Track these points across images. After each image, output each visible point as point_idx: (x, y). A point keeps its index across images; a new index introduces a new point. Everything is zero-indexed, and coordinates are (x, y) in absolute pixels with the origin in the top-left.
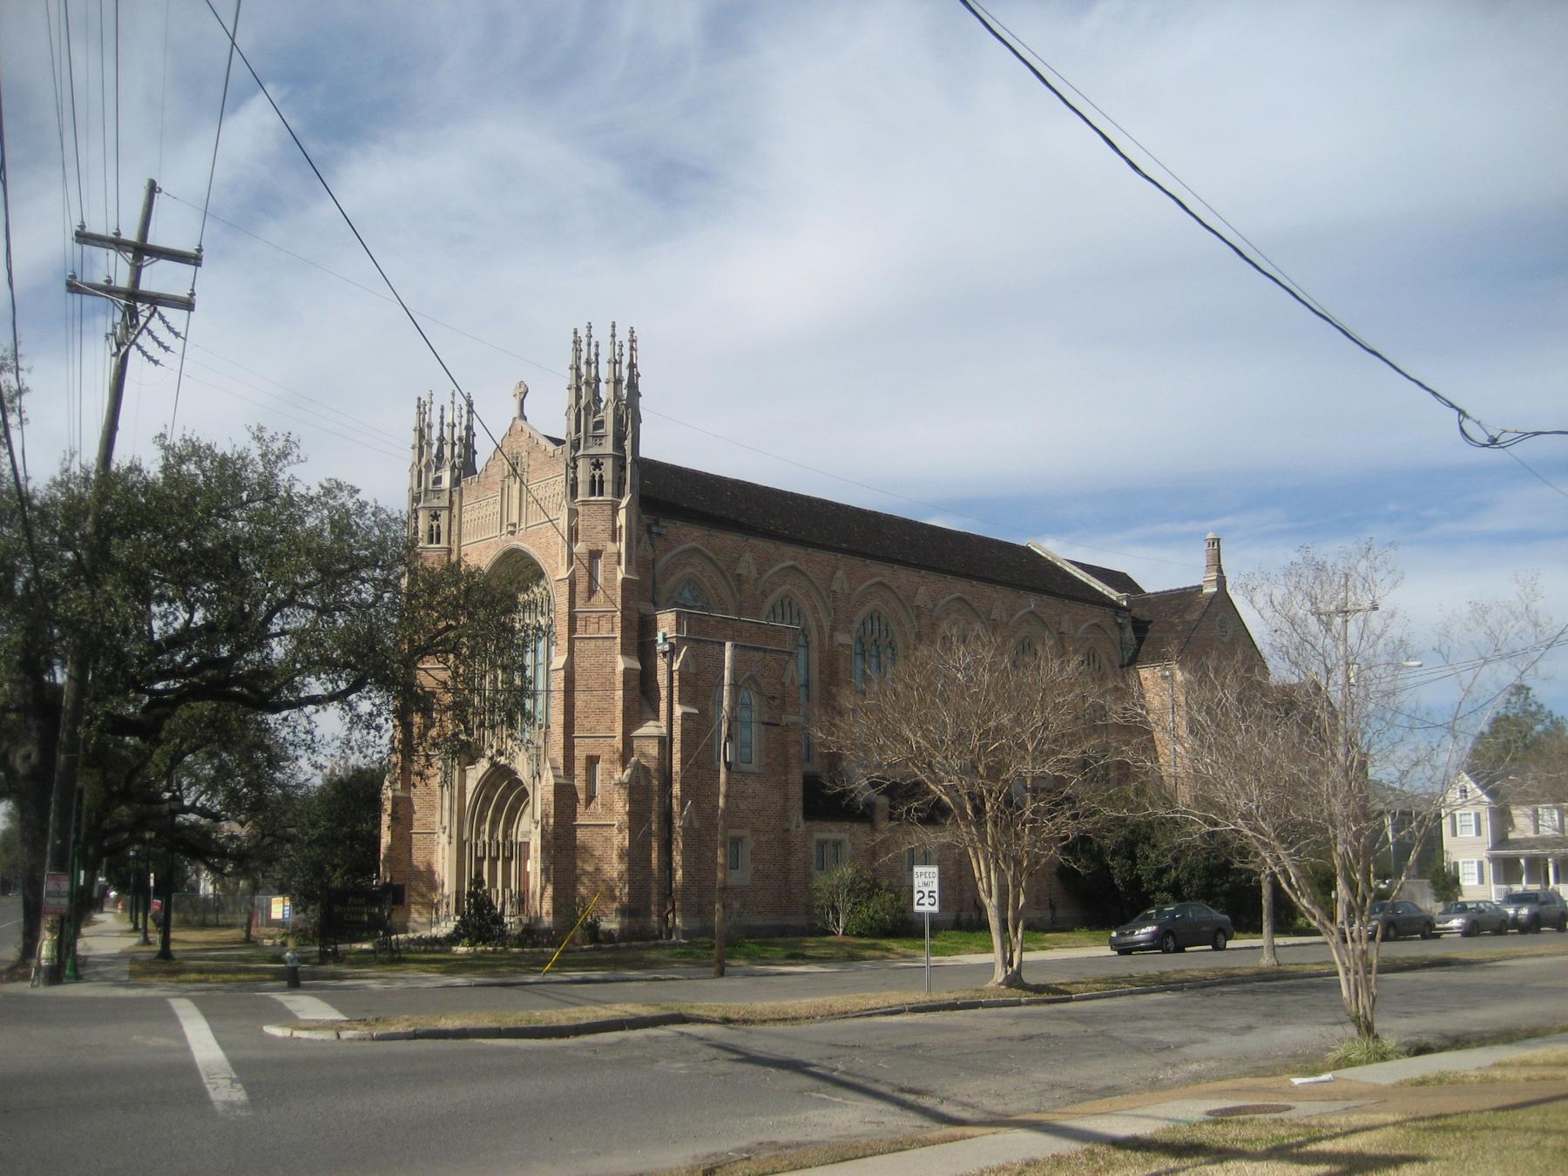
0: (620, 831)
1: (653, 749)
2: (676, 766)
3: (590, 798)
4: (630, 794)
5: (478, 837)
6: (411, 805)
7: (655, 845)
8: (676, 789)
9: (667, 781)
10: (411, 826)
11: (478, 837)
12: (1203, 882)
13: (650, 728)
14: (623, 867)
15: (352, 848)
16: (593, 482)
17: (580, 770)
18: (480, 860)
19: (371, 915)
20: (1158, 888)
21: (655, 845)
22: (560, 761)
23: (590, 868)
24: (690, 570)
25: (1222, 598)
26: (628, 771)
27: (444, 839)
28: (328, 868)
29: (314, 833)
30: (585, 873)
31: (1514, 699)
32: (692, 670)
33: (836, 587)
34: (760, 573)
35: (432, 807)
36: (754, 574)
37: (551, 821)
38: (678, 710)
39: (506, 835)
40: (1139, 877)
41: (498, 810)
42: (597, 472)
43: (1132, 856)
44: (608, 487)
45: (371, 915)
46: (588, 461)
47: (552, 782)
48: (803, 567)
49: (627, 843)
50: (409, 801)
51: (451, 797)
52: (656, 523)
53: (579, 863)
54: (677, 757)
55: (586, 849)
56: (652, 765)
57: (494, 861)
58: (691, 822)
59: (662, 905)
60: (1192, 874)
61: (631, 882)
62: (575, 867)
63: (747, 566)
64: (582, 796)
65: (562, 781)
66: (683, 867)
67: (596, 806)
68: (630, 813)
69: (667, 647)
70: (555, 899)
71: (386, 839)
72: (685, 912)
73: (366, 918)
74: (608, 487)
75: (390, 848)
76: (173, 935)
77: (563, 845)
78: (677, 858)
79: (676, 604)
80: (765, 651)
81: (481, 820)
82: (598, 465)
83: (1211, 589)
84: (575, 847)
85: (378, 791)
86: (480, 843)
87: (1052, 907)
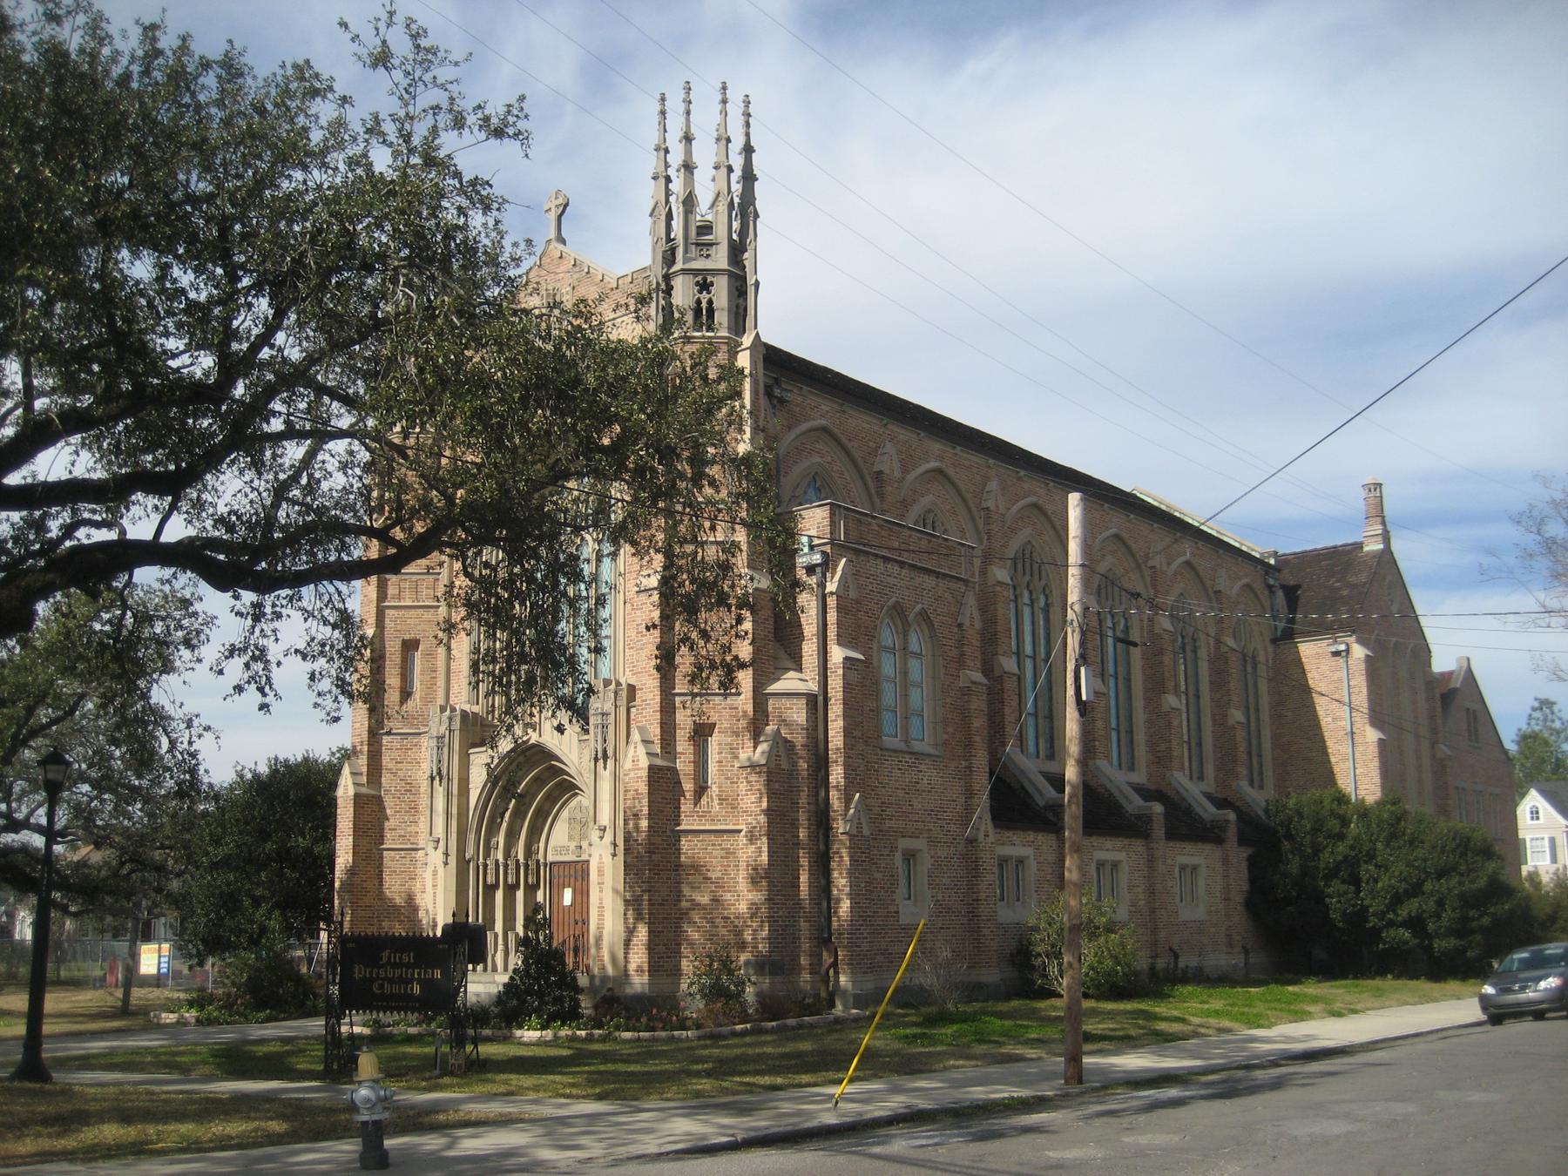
0: (752, 838)
1: (798, 714)
2: (836, 738)
3: (701, 790)
4: (769, 782)
5: (487, 855)
6: (382, 808)
7: (804, 862)
8: (837, 775)
9: (821, 763)
10: (381, 838)
11: (487, 855)
12: (1457, 914)
13: (789, 682)
14: (758, 896)
15: (280, 875)
16: (698, 311)
17: (683, 746)
18: (490, 889)
19: (425, 984)
20: (1391, 924)
21: (804, 862)
22: (655, 731)
23: (704, 899)
24: (816, 459)
25: (1386, 558)
26: (763, 747)
27: (436, 857)
28: (247, 902)
29: (220, 853)
30: (696, 906)
31: (1537, 714)
32: (852, 594)
33: (990, 504)
34: (905, 470)
35: (414, 809)
36: (897, 474)
37: (644, 824)
38: (837, 654)
39: (529, 852)
40: (1364, 909)
41: (519, 814)
42: (704, 297)
43: (1355, 881)
44: (721, 318)
45: (427, 984)
46: (690, 280)
47: (644, 762)
48: (951, 472)
49: (765, 858)
50: (379, 801)
51: (448, 794)
52: (777, 381)
53: (686, 890)
54: (836, 726)
55: (696, 868)
56: (799, 739)
57: (511, 890)
58: (859, 826)
59: (816, 956)
60: (1441, 903)
61: (772, 919)
62: (679, 897)
63: (888, 463)
64: (688, 786)
65: (659, 762)
66: (851, 896)
67: (712, 799)
68: (768, 812)
69: (817, 558)
70: (651, 948)
71: (344, 857)
72: (855, 967)
73: (417, 989)
74: (721, 318)
75: (351, 872)
76: (21, 1029)
77: (657, 866)
78: (841, 881)
79: (832, 494)
80: (937, 574)
81: (492, 830)
82: (705, 286)
83: (1374, 546)
84: (678, 866)
85: (333, 785)
86: (491, 866)
87: (1246, 951)
